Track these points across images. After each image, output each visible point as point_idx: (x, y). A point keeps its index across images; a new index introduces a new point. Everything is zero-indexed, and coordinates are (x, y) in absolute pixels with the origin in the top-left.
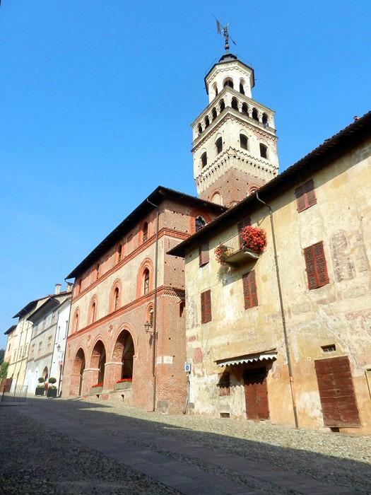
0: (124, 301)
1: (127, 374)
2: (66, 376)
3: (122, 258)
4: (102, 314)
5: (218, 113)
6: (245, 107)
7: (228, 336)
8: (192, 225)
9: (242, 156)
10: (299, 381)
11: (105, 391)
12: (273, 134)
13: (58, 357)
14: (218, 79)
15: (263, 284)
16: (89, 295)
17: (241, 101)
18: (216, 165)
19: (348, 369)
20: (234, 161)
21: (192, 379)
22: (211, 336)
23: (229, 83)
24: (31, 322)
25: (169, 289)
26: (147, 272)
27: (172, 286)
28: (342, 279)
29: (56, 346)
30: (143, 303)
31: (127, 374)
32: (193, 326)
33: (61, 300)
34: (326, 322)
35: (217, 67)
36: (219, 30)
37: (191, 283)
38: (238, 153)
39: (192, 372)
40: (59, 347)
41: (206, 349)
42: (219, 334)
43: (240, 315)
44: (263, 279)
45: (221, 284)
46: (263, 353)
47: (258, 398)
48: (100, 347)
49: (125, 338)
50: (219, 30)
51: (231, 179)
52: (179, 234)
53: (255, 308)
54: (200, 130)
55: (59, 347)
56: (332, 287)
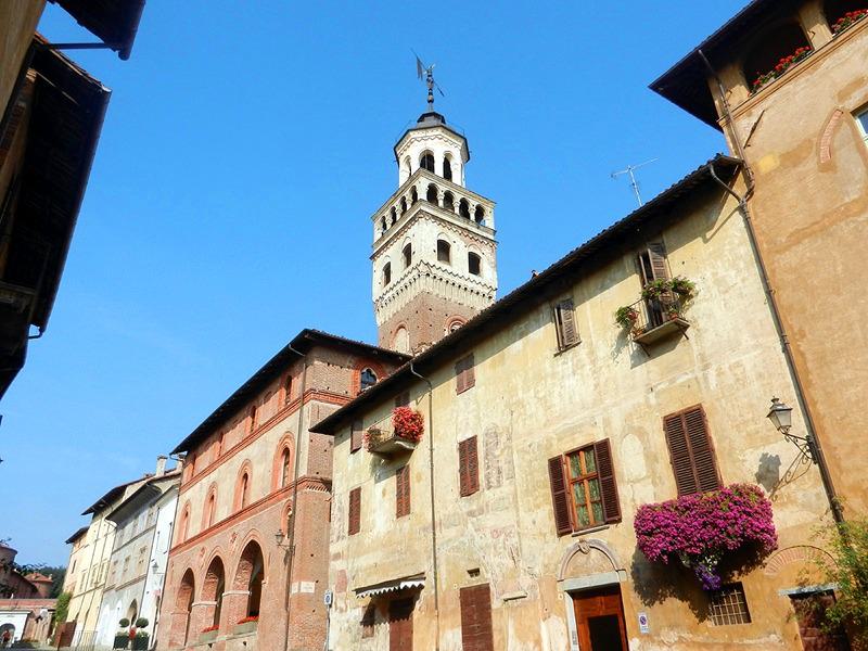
0: (255, 495)
1: (253, 611)
2: (166, 614)
3: (256, 427)
4: (222, 514)
6: (449, 197)
8: (355, 382)
9: (439, 273)
10: (445, 616)
11: (222, 637)
12: (491, 237)
13: (153, 584)
14: (413, 152)
15: (417, 484)
16: (206, 482)
17: (442, 189)
19: (488, 599)
20: (421, 281)
21: (334, 614)
22: (358, 554)
23: (427, 161)
24: (112, 522)
25: (315, 480)
26: (286, 452)
27: (319, 476)
31: (253, 611)
32: (338, 538)
33: (164, 487)
35: (411, 133)
36: (420, 72)
38: (434, 270)
40: (156, 566)
45: (373, 481)
46: (405, 579)
47: (402, 640)
48: (217, 567)
49: (253, 553)
50: (420, 72)
51: (423, 308)
52: (335, 397)
53: (407, 517)
54: (385, 226)
55: (156, 566)
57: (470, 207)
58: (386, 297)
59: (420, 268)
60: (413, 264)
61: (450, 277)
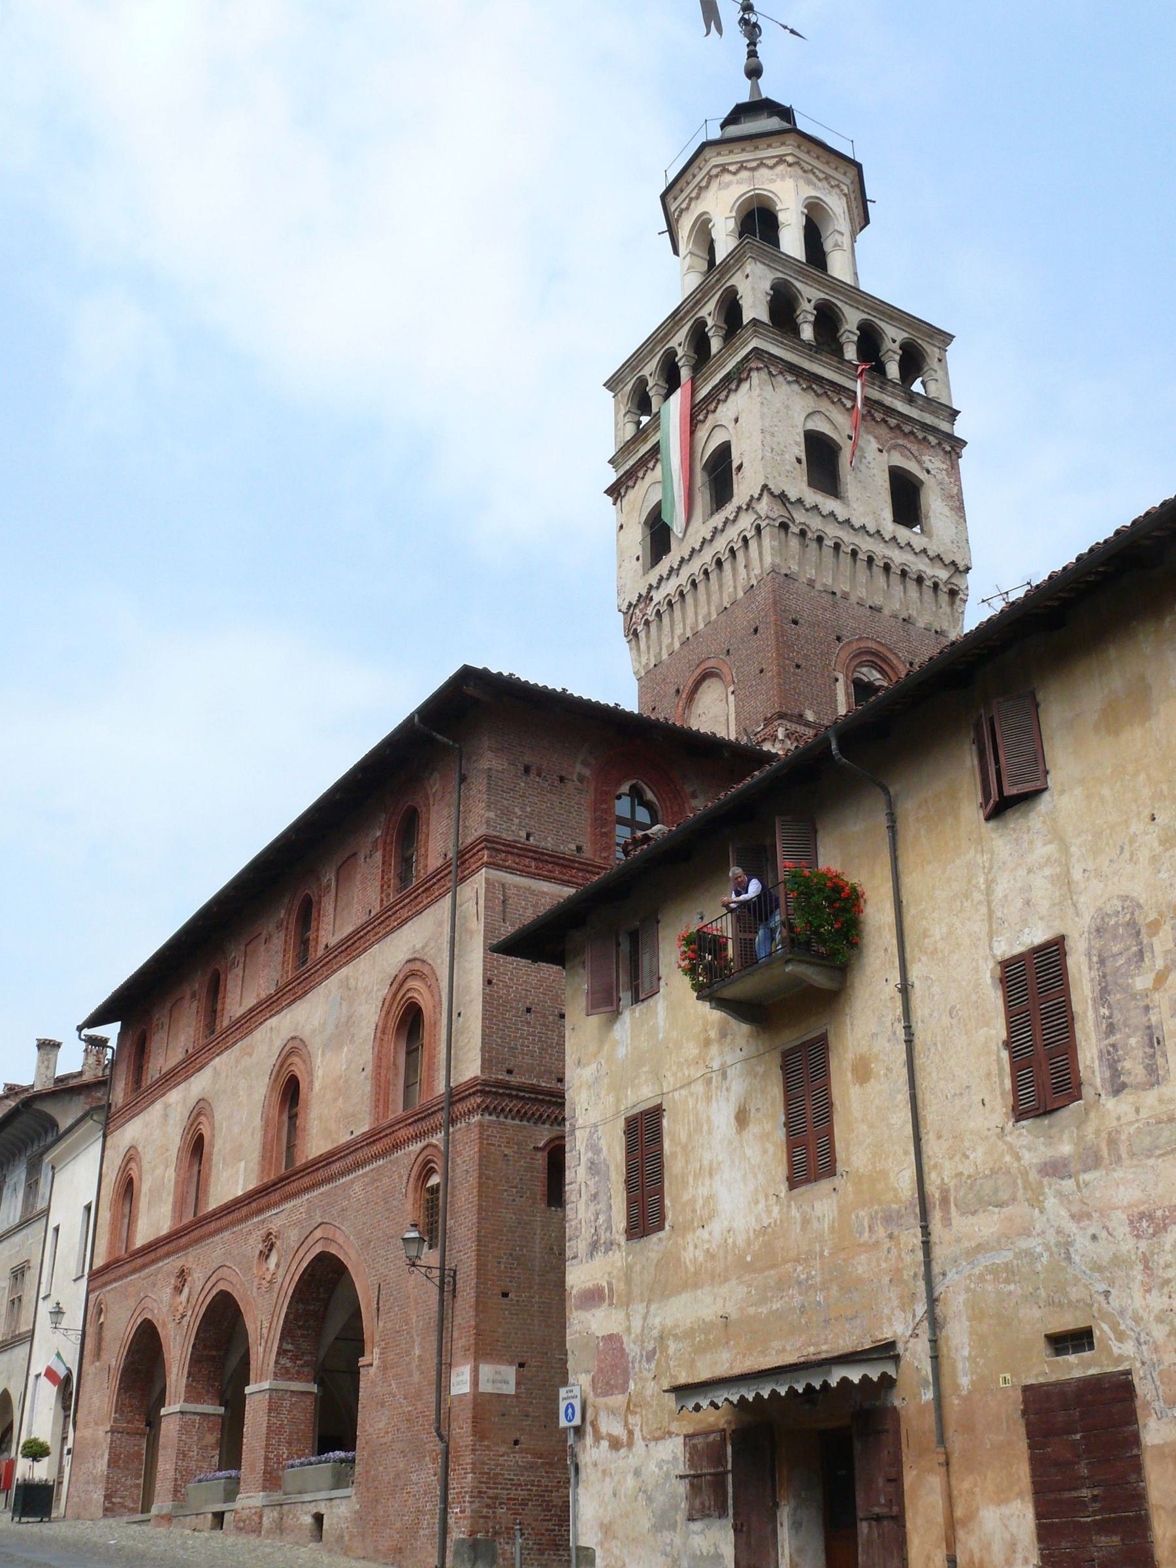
0: (321, 1132)
5: (715, 345)
6: (827, 319)
7: (724, 1290)
15: (855, 1091)
17: (809, 294)
18: (707, 557)
21: (591, 1454)
28: (1124, 1086)
29: (45, 1308)
30: (396, 1146)
32: (594, 1246)
34: (1067, 1245)
37: (588, 1073)
39: (589, 1429)
40: (58, 1312)
41: (641, 1340)
42: (692, 1283)
43: (769, 1212)
44: (855, 1070)
53: (825, 1185)
56: (1092, 1115)
57: (888, 345)
58: (658, 596)
59: (763, 507)
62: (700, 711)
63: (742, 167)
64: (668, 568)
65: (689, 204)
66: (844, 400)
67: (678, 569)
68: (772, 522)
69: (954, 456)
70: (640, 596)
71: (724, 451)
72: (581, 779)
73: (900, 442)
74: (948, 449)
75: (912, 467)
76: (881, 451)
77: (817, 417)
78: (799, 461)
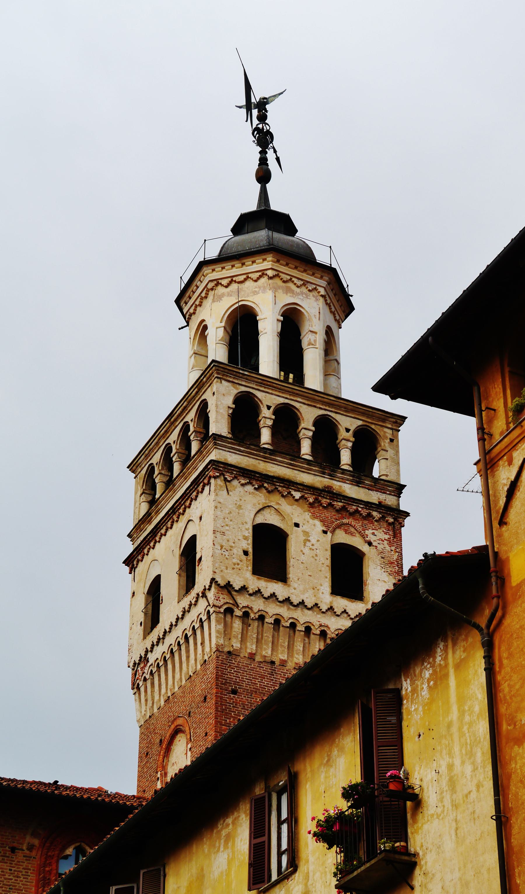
57: (342, 434)
60: (198, 588)
61: (285, 612)
62: (173, 761)
63: (232, 280)
64: (156, 637)
65: (195, 310)
66: (293, 493)
67: (163, 638)
68: (218, 609)
69: (397, 526)
70: (141, 657)
71: (193, 539)
72: (31, 848)
73: (345, 521)
74: (391, 520)
75: (356, 542)
76: (325, 532)
77: (266, 512)
78: (246, 553)
